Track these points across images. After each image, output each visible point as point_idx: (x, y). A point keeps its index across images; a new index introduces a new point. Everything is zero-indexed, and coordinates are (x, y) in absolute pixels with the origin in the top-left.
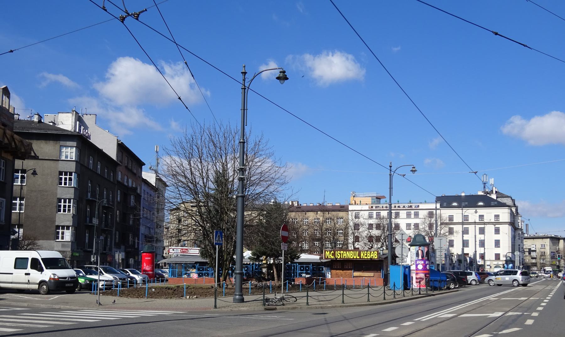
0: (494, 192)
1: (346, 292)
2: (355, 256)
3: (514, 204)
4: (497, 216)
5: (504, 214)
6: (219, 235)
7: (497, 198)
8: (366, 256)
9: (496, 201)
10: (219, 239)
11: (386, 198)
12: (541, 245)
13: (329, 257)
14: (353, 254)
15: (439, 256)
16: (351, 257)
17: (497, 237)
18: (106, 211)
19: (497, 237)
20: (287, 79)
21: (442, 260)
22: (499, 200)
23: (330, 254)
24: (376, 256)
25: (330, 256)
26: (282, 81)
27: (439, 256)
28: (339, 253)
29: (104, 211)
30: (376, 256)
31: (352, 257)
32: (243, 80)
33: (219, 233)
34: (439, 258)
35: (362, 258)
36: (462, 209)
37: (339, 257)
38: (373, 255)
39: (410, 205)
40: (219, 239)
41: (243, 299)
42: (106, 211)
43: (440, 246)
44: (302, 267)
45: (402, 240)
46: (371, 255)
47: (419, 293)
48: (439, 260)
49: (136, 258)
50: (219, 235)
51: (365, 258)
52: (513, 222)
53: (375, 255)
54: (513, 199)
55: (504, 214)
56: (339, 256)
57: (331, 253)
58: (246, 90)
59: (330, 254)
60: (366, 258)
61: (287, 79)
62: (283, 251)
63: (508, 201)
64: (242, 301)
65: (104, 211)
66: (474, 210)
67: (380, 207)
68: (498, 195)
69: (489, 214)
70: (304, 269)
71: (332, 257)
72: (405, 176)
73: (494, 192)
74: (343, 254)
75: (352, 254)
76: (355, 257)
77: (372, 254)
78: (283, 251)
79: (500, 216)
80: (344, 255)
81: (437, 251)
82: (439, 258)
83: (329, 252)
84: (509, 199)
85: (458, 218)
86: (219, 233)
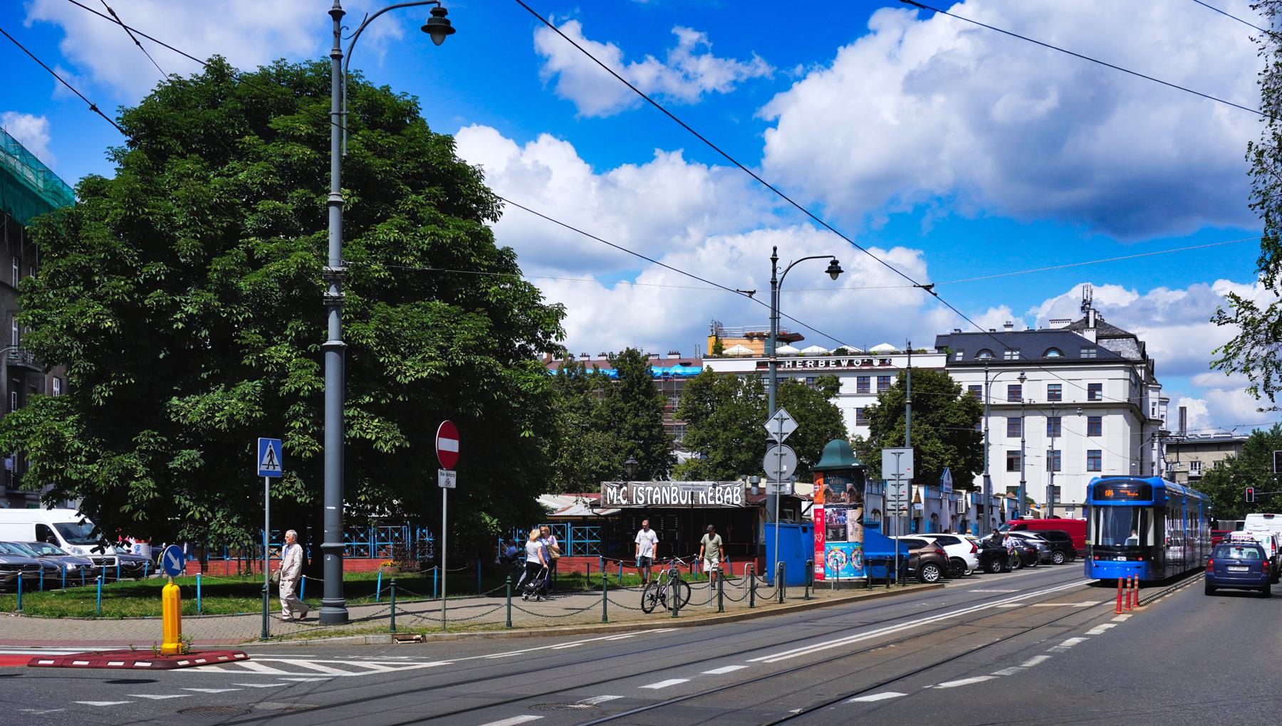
0: (1091, 324)
1: (610, 594)
2: (683, 499)
3: (1144, 354)
4: (1094, 389)
5: (1115, 386)
6: (271, 451)
7: (1097, 338)
8: (713, 498)
9: (1095, 346)
10: (271, 460)
11: (803, 339)
12: (1192, 462)
13: (615, 502)
14: (678, 494)
15: (894, 498)
16: (673, 502)
17: (1094, 443)
18: (18, 381)
19: (1094, 443)
20: (452, 31)
21: (901, 508)
22: (1104, 343)
23: (618, 494)
24: (737, 498)
25: (618, 500)
26: (438, 38)
27: (894, 498)
28: (641, 491)
29: (14, 379)
30: (737, 498)
31: (676, 502)
32: (335, 33)
33: (270, 444)
34: (894, 503)
35: (703, 505)
36: (987, 372)
37: (641, 502)
38: (730, 496)
39: (866, 358)
40: (271, 460)
41: (346, 615)
42: (18, 381)
43: (895, 473)
44: (579, 530)
45: (781, 455)
46: (726, 497)
47: (803, 595)
48: (893, 508)
49: (978, 481)
50: (271, 450)
51: (710, 502)
52: (1136, 400)
53: (735, 496)
54: (1140, 340)
55: (1115, 386)
56: (641, 499)
57: (622, 490)
58: (343, 60)
59: (618, 494)
60: (713, 502)
61: (452, 31)
62: (445, 490)
63: (1129, 351)
64: (344, 619)
65: (14, 379)
66: (1018, 374)
67: (787, 364)
68: (1102, 330)
69: (1074, 386)
70: (387, 534)
71: (624, 502)
72: (754, 296)
73: (1091, 324)
74: (652, 492)
75: (675, 494)
76: (683, 502)
77: (728, 493)
78: (445, 490)
79: (1104, 388)
80: (655, 497)
81: (889, 483)
82: (894, 503)
83: (615, 489)
84: (1131, 342)
85: (999, 395)
86: (270, 444)
